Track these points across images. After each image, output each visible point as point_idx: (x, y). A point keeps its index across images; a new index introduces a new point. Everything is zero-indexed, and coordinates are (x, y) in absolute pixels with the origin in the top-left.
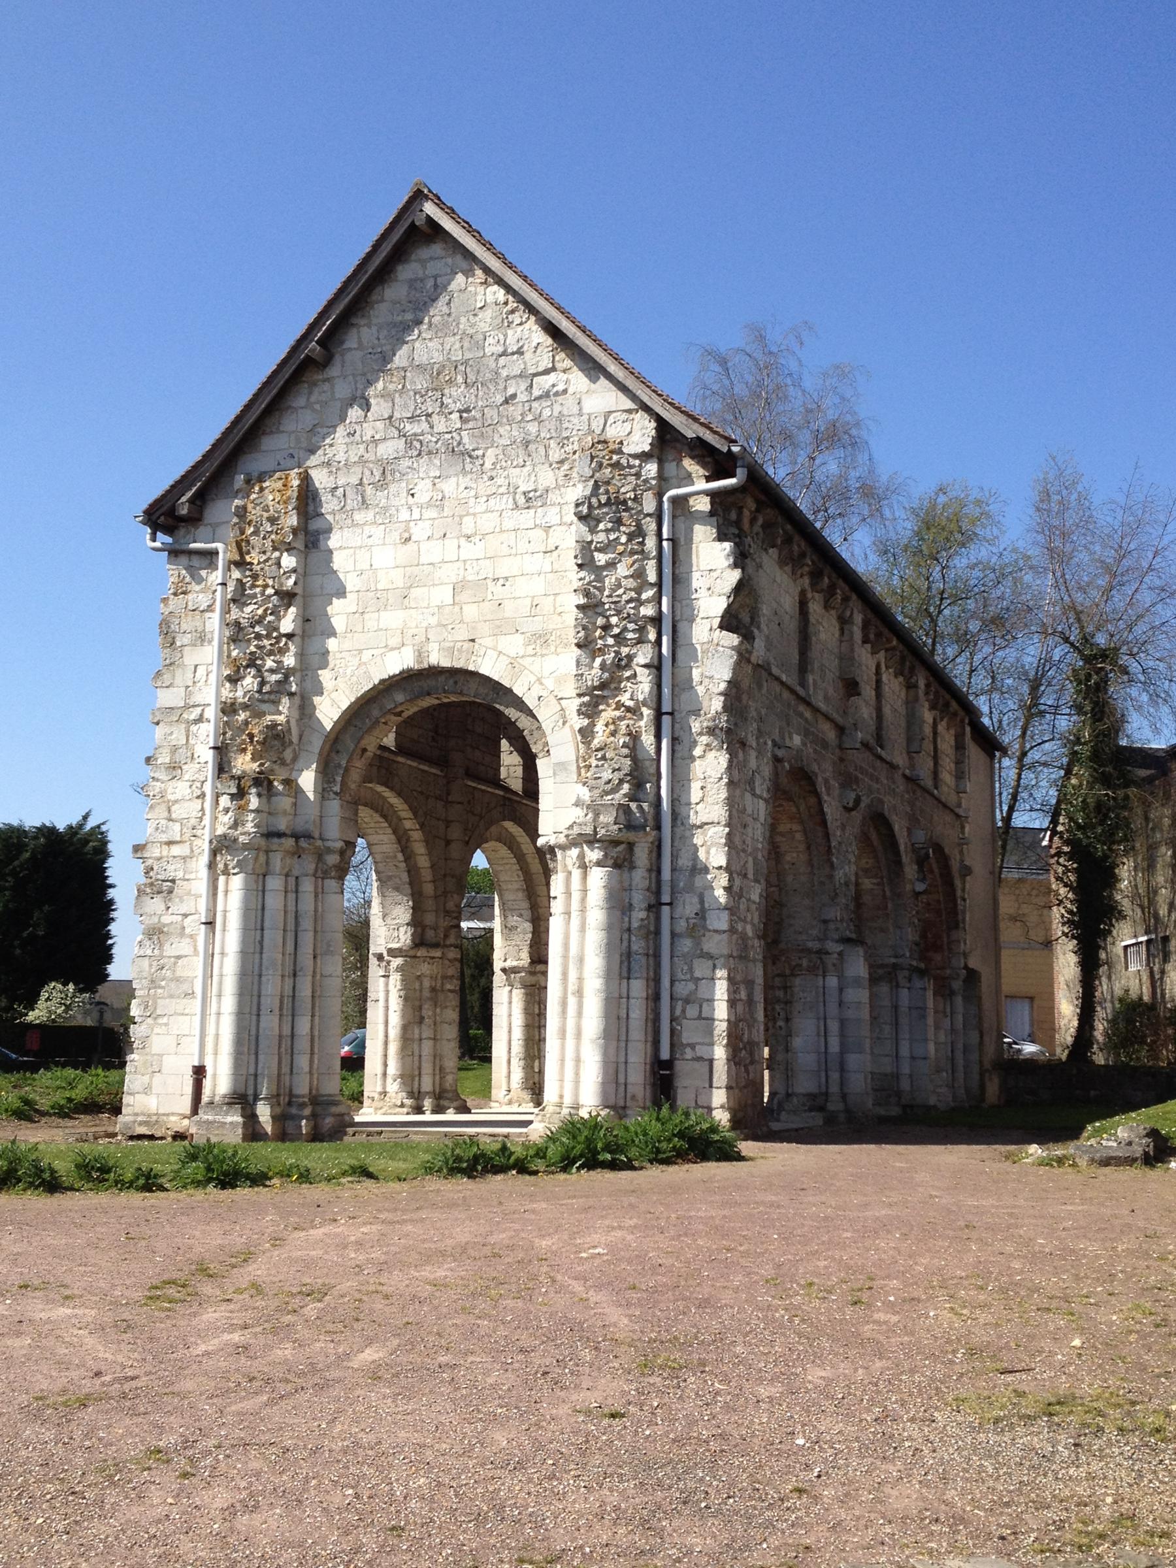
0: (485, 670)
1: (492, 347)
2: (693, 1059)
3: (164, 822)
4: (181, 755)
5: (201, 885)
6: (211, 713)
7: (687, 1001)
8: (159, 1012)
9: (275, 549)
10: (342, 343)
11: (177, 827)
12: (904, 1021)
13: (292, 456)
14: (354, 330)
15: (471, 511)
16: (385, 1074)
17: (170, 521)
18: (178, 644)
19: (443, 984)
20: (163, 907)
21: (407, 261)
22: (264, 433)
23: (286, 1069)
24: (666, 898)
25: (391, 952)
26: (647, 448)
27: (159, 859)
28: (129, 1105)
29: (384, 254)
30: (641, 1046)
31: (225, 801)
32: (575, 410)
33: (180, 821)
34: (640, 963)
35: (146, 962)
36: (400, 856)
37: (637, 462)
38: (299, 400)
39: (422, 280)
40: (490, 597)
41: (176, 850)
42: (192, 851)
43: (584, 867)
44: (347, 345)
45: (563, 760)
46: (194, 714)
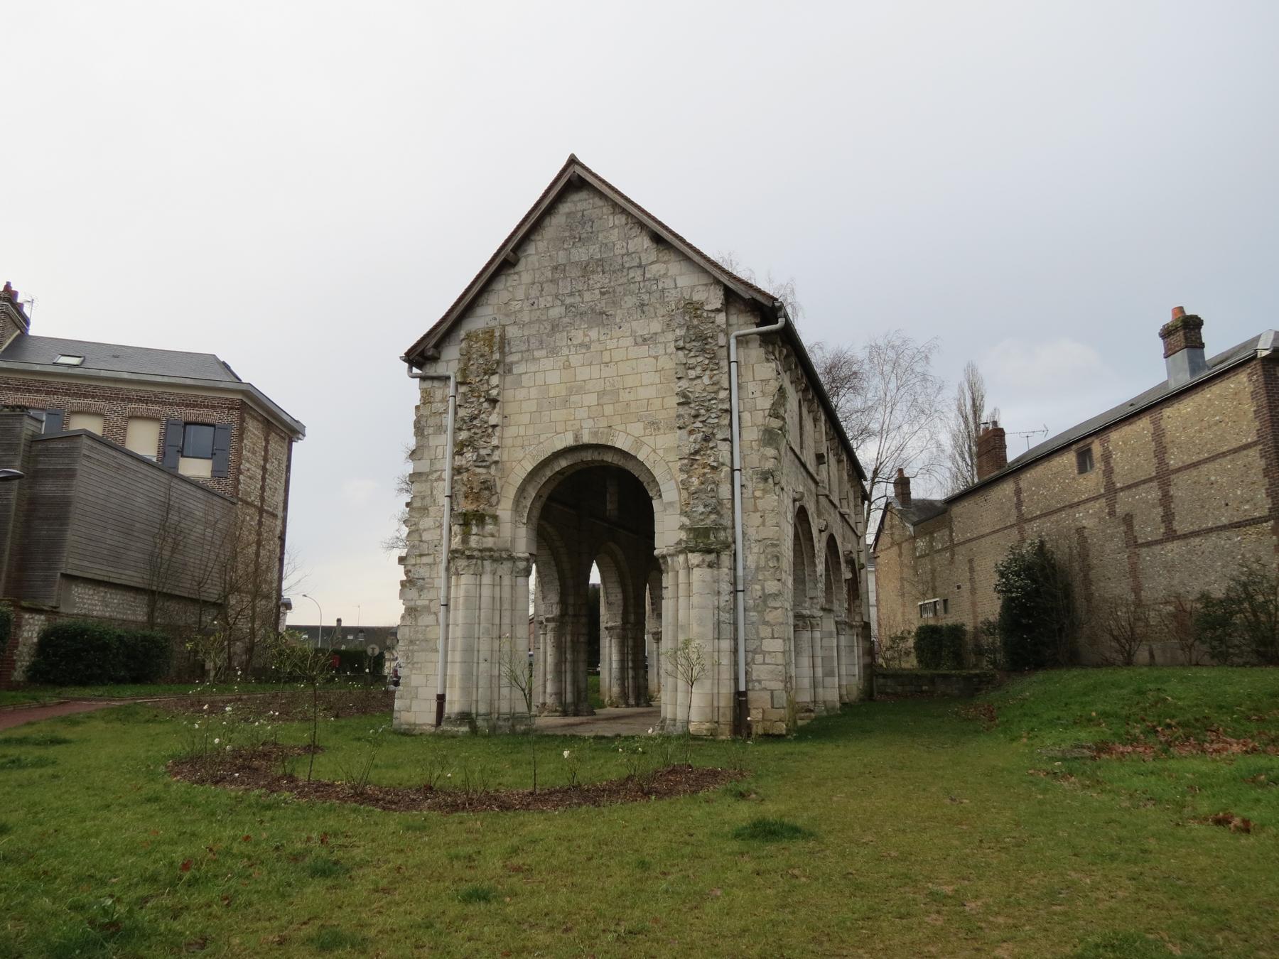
0: (618, 445)
1: (619, 250)
2: (760, 690)
3: (417, 543)
4: (428, 501)
5: (441, 582)
6: (447, 475)
7: (755, 652)
8: (415, 660)
9: (485, 374)
10: (525, 251)
11: (425, 545)
12: (843, 654)
13: (495, 319)
14: (533, 243)
15: (608, 347)
16: (545, 692)
17: (421, 360)
18: (426, 433)
19: (578, 639)
20: (417, 595)
21: (565, 202)
22: (478, 306)
23: (496, 696)
24: (740, 587)
25: (548, 620)
26: (719, 306)
27: (414, 565)
28: (397, 718)
29: (551, 199)
30: (727, 682)
31: (456, 528)
32: (672, 285)
33: (427, 542)
34: (727, 629)
35: (407, 629)
36: (553, 563)
37: (713, 315)
38: (499, 285)
39: (574, 213)
40: (621, 399)
41: (425, 560)
42: (435, 560)
43: (689, 569)
44: (528, 252)
45: (670, 500)
46: (435, 475)
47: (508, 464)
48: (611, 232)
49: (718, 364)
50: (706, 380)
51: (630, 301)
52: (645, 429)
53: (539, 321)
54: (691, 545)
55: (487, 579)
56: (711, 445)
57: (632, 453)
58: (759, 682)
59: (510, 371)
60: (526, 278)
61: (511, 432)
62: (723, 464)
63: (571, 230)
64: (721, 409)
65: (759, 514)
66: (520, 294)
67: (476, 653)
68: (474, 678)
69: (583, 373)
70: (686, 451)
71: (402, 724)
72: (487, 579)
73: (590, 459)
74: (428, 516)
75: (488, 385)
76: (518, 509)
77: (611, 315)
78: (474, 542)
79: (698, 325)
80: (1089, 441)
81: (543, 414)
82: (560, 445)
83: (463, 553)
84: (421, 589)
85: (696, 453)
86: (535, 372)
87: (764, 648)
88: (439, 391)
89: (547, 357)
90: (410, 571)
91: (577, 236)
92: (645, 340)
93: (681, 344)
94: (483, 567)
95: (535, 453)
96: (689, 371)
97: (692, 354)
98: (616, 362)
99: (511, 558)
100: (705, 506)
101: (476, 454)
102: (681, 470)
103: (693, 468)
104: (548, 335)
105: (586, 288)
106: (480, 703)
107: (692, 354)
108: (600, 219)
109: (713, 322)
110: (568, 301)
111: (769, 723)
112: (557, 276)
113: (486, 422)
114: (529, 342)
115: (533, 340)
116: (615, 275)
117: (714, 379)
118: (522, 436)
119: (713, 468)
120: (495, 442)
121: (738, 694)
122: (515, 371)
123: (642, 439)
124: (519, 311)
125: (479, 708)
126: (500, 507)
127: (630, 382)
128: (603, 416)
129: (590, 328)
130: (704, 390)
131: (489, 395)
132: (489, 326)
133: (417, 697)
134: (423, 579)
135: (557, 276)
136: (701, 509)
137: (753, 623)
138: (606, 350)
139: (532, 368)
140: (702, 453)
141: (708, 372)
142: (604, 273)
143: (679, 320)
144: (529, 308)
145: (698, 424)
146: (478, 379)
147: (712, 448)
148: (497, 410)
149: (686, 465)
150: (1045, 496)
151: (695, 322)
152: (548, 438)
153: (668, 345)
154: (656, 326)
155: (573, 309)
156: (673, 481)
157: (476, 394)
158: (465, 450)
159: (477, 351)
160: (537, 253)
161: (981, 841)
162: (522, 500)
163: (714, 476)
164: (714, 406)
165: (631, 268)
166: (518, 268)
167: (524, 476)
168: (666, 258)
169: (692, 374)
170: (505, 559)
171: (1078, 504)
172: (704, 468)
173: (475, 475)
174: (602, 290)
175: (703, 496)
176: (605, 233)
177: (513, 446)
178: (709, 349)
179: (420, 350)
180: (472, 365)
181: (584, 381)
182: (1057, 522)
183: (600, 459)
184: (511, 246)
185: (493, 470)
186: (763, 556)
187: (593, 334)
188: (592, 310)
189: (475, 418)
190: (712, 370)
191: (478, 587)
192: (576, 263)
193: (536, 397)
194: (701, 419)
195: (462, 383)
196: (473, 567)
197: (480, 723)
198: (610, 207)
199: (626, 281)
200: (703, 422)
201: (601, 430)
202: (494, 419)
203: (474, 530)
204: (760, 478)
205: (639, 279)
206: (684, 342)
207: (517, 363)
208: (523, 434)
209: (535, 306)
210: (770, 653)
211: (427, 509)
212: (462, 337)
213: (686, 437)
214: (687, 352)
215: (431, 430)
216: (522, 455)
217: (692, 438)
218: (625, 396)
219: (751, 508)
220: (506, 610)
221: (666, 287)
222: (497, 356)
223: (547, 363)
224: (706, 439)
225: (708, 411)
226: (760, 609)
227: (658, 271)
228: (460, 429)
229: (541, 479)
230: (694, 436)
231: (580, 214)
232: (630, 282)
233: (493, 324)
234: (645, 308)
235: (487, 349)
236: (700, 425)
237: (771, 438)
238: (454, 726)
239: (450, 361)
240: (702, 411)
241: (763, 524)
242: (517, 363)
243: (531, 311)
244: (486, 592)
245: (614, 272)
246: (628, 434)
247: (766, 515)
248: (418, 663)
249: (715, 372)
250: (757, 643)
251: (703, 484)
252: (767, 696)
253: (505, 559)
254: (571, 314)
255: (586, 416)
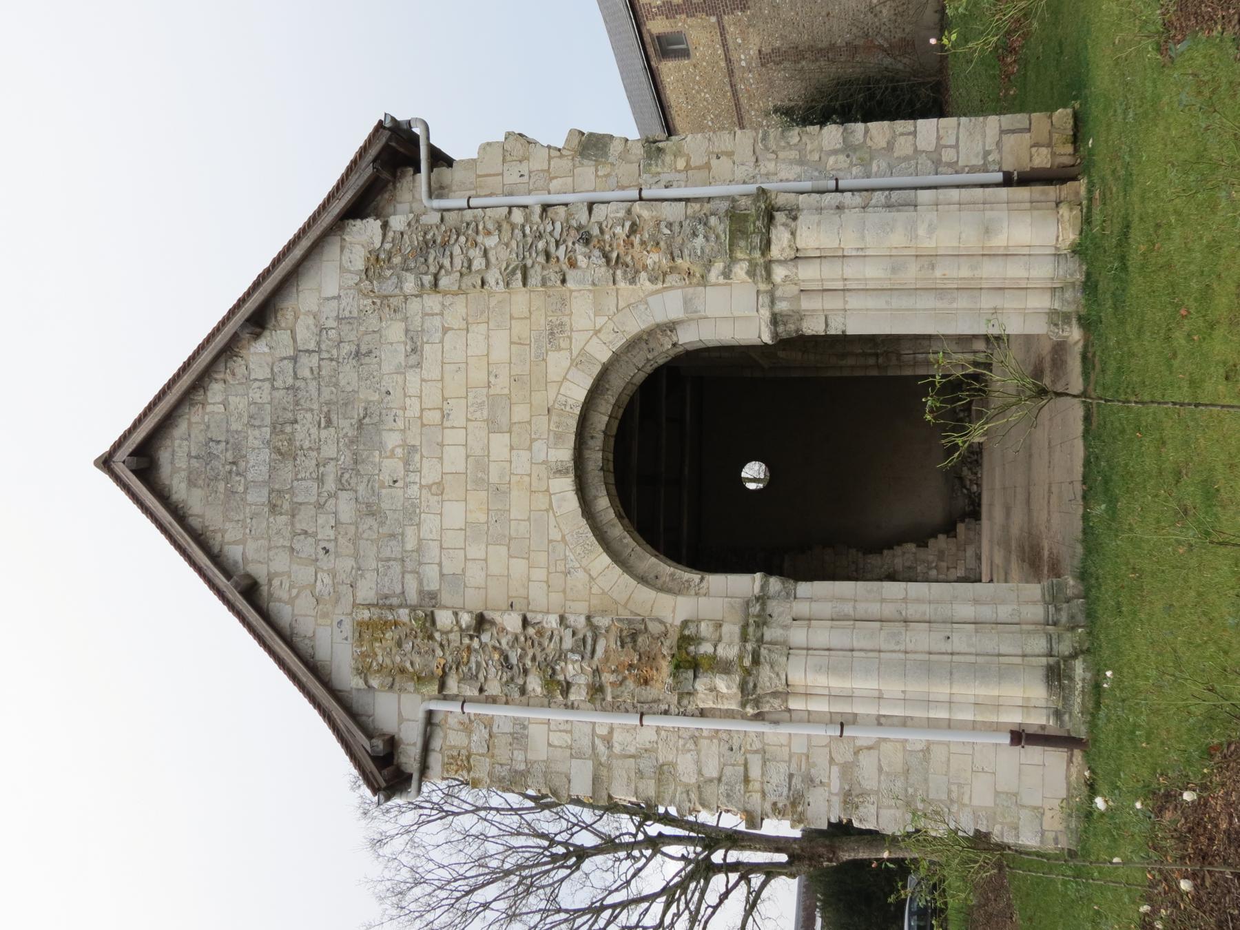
1: (261, 394)
3: (722, 788)
4: (646, 764)
6: (603, 720)
7: (937, 163)
9: (431, 637)
10: (236, 563)
11: (728, 771)
13: (340, 623)
14: (226, 548)
18: (523, 767)
20: (820, 790)
26: (379, 223)
27: (764, 794)
32: (334, 303)
35: (883, 812)
37: (390, 234)
38: (284, 613)
39: (190, 473)
40: (506, 391)
41: (755, 772)
42: (756, 752)
44: (239, 558)
46: (601, 748)
47: (594, 601)
48: (232, 407)
49: (468, 224)
50: (491, 242)
51: (348, 376)
52: (559, 349)
53: (355, 540)
54: (757, 240)
55: (798, 636)
56: (595, 231)
57: (597, 369)
58: (987, 153)
59: (433, 596)
60: (280, 562)
61: (538, 595)
62: (629, 212)
63: (216, 479)
64: (541, 217)
65: (714, 162)
66: (304, 574)
67: (933, 657)
68: (980, 659)
69: (455, 459)
70: (602, 271)
71: (1068, 827)
72: (798, 636)
73: (600, 454)
74: (673, 765)
75: (451, 631)
76: (677, 589)
77: (366, 409)
78: (728, 651)
79: (403, 255)
80: (647, 39)
81: (513, 534)
82: (572, 503)
83: (748, 672)
84: (810, 781)
85: (606, 256)
86: (441, 547)
87: (931, 148)
88: (449, 739)
89: (418, 525)
90: (775, 804)
91: (228, 467)
92: (414, 350)
93: (428, 279)
94: (775, 643)
95: (579, 549)
96: (474, 268)
97: (447, 262)
98: (444, 399)
99: (762, 599)
100: (695, 235)
101: (570, 654)
102: (633, 281)
103: (631, 263)
104: (382, 524)
105: (315, 453)
106: (1028, 650)
107: (447, 262)
108: (208, 427)
109: (402, 234)
110: (330, 485)
111: (1056, 136)
112: (286, 506)
113: (516, 639)
114: (389, 559)
115: (386, 553)
116: (302, 402)
117: (491, 226)
118: (549, 573)
119: (634, 229)
120: (552, 622)
121: (1008, 181)
122: (433, 586)
123: (575, 353)
124: (334, 577)
125: (1037, 651)
126: (669, 620)
127: (479, 376)
128: (529, 423)
129: (381, 446)
130: (507, 245)
131: (468, 628)
132: (350, 635)
133: (1016, 795)
134: (791, 776)
135: (286, 506)
136: (700, 241)
137: (890, 167)
138: (421, 417)
139: (433, 552)
140: (607, 248)
141: (480, 239)
142: (296, 422)
143: (389, 287)
144: (332, 557)
145: (561, 252)
146: (439, 652)
147: (602, 231)
148: (496, 616)
149: (625, 272)
150: (716, 116)
151: (397, 260)
152: (558, 526)
153: (428, 310)
154: (395, 331)
155: (347, 476)
156: (650, 299)
157: (465, 655)
158: (561, 677)
159: (389, 654)
160: (243, 542)
161: (1158, 522)
162: (659, 583)
163: (646, 228)
164: (535, 228)
165: (295, 373)
166: (263, 580)
167: (618, 570)
168: (290, 315)
169: (478, 263)
170: (763, 609)
171: (728, 60)
172: (632, 245)
173: (607, 659)
174: (323, 425)
175: (679, 240)
176: (233, 419)
177: (564, 591)
178: (443, 237)
179: (370, 766)
180: (412, 664)
181: (467, 457)
182: (749, 98)
183: (600, 436)
184: (221, 579)
185: (602, 622)
186: (782, 155)
187: (392, 440)
188: (352, 442)
189: (506, 658)
190: (477, 233)
191: (810, 652)
192: (272, 469)
193: (483, 547)
194: (552, 248)
195: (442, 686)
196: (775, 656)
197: (1065, 648)
198: (194, 410)
199: (315, 383)
200: (557, 244)
201: (553, 427)
202: (512, 622)
203: (707, 648)
204: (656, 160)
205: (315, 359)
206: (426, 274)
207: (421, 583)
208: (544, 572)
209: (331, 546)
210: (939, 138)
211: (662, 766)
212: (361, 684)
213: (579, 272)
214: (443, 272)
215: (519, 756)
216: (581, 575)
217: (582, 261)
218: (501, 385)
219: (704, 173)
220: (854, 608)
221: (335, 314)
222: (404, 614)
223: (430, 525)
224: (586, 240)
225: (540, 237)
226: (867, 156)
227: (308, 328)
228: (523, 691)
229: (627, 545)
230: (580, 258)
231: (193, 461)
232: (317, 374)
233: (348, 627)
234: (364, 349)
235: (389, 635)
236: (562, 248)
237: (595, 145)
238: (1072, 689)
239: (400, 713)
240: (541, 245)
241: (730, 154)
242: (421, 583)
243: (337, 555)
244: (822, 636)
245: (297, 403)
246: (565, 378)
247: (716, 150)
248: (949, 792)
249: (481, 227)
250: (923, 159)
251: (658, 244)
252: (1010, 139)
253: (763, 609)
254: (353, 481)
255: (525, 455)
